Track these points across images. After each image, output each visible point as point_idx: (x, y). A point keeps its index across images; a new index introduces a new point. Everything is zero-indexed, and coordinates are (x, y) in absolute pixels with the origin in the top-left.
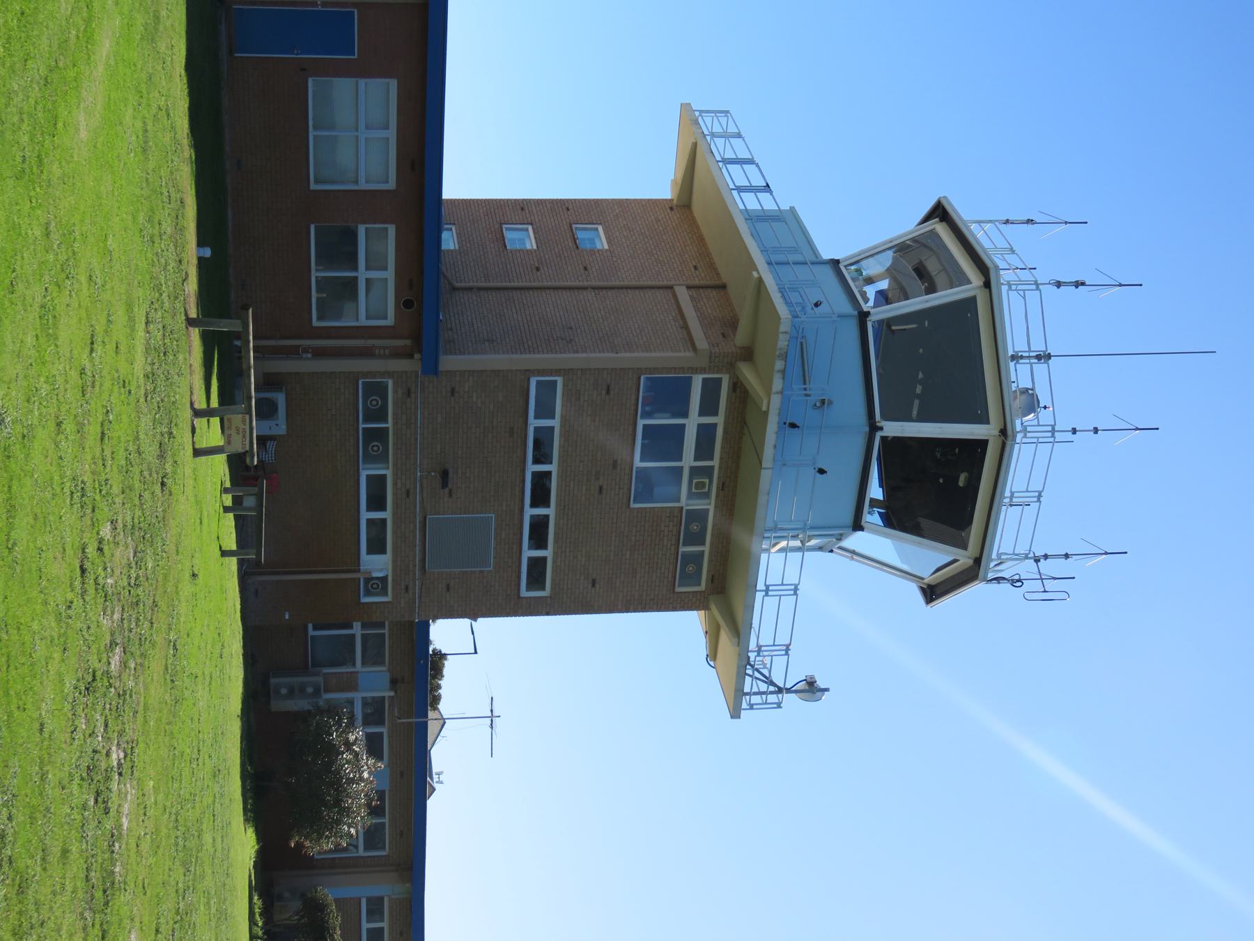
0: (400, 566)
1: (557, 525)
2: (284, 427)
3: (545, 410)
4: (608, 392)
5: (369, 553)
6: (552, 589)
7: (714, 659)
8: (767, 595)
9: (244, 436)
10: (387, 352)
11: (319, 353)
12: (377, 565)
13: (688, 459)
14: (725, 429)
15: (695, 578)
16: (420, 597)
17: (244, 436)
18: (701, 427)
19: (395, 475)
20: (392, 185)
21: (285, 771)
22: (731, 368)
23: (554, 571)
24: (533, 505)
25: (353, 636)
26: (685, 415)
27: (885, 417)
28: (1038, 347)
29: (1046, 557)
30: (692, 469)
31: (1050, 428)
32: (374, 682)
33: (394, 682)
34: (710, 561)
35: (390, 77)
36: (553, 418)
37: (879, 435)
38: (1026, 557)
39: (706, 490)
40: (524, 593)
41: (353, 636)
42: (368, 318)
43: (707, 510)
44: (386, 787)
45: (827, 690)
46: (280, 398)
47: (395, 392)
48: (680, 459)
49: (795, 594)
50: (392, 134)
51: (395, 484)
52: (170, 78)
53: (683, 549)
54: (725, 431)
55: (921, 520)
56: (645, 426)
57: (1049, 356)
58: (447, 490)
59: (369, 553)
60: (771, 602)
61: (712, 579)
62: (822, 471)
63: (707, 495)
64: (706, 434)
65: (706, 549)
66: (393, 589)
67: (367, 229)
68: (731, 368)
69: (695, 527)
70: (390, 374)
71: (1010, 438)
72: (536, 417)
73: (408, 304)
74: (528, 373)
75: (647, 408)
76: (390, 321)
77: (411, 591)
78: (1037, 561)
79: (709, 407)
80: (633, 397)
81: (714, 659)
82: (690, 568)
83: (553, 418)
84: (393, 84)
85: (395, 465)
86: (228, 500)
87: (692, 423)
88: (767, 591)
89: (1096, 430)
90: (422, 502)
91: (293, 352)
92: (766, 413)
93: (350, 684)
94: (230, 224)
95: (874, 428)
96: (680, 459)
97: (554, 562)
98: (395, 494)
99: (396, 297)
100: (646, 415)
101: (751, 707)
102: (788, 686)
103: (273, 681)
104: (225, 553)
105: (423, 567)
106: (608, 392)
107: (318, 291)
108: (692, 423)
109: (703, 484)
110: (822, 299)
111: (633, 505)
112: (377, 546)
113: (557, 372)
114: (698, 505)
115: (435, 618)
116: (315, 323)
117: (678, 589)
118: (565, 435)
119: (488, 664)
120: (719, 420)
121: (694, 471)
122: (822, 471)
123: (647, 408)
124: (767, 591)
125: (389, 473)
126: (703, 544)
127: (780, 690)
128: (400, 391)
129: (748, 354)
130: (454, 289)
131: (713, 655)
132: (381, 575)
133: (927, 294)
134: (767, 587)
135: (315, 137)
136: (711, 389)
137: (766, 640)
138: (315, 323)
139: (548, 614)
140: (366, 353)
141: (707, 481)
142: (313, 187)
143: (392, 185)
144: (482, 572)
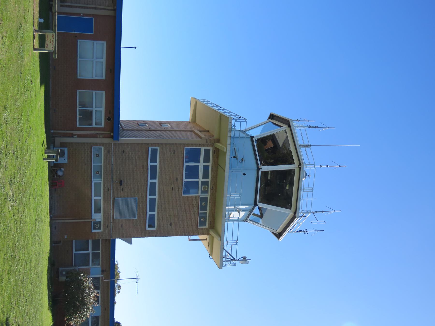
0: (106, 218)
1: (158, 202)
2: (67, 160)
3: (154, 160)
5: (95, 213)
6: (157, 226)
7: (212, 255)
8: (227, 244)
9: (53, 44)
11: (79, 136)
12: (98, 217)
13: (200, 179)
15: (204, 223)
17: (53, 44)
19: (104, 183)
20: (104, 78)
21: (64, 296)
26: (199, 162)
27: (260, 202)
28: (306, 143)
29: (316, 212)
30: (202, 182)
32: (96, 270)
33: (103, 271)
34: (209, 216)
35: (104, 40)
36: (156, 162)
37: (260, 171)
40: (148, 229)
41: (89, 254)
42: (96, 76)
44: (99, 314)
46: (66, 150)
47: (104, 151)
48: (198, 178)
49: (236, 244)
50: (104, 60)
51: (104, 186)
52: (38, 220)
53: (200, 212)
54: (212, 168)
55: (281, 145)
56: (187, 166)
57: (310, 145)
59: (95, 213)
60: (230, 224)
61: (210, 223)
62: (244, 174)
63: (207, 192)
64: (206, 168)
65: (208, 212)
68: (213, 145)
72: (150, 195)
73: (109, 119)
74: (148, 145)
75: (187, 160)
76: (103, 126)
78: (313, 213)
79: (206, 160)
81: (212, 255)
83: (155, 211)
84: (105, 43)
85: (104, 178)
86: (46, 156)
87: (201, 165)
89: (322, 212)
90: (113, 193)
91: (70, 135)
92: (226, 152)
94: (51, 88)
95: (259, 169)
96: (198, 178)
97: (158, 216)
98: (104, 190)
99: (105, 117)
100: (186, 162)
101: (226, 265)
102: (238, 258)
105: (113, 218)
106: (174, 153)
107: (79, 115)
108: (201, 165)
109: (206, 187)
111: (183, 195)
112: (98, 211)
113: (157, 145)
114: (204, 195)
115: (117, 238)
116: (78, 126)
117: (199, 227)
118: (161, 168)
119: (132, 255)
120: (210, 164)
122: (244, 174)
124: (227, 243)
126: (206, 210)
127: (234, 260)
129: (218, 141)
130: (123, 130)
131: (211, 254)
132: (99, 220)
136: (207, 152)
137: (229, 239)
138: (78, 126)
139: (156, 236)
140: (95, 136)
142: (78, 78)
143: (104, 78)
144: (133, 220)
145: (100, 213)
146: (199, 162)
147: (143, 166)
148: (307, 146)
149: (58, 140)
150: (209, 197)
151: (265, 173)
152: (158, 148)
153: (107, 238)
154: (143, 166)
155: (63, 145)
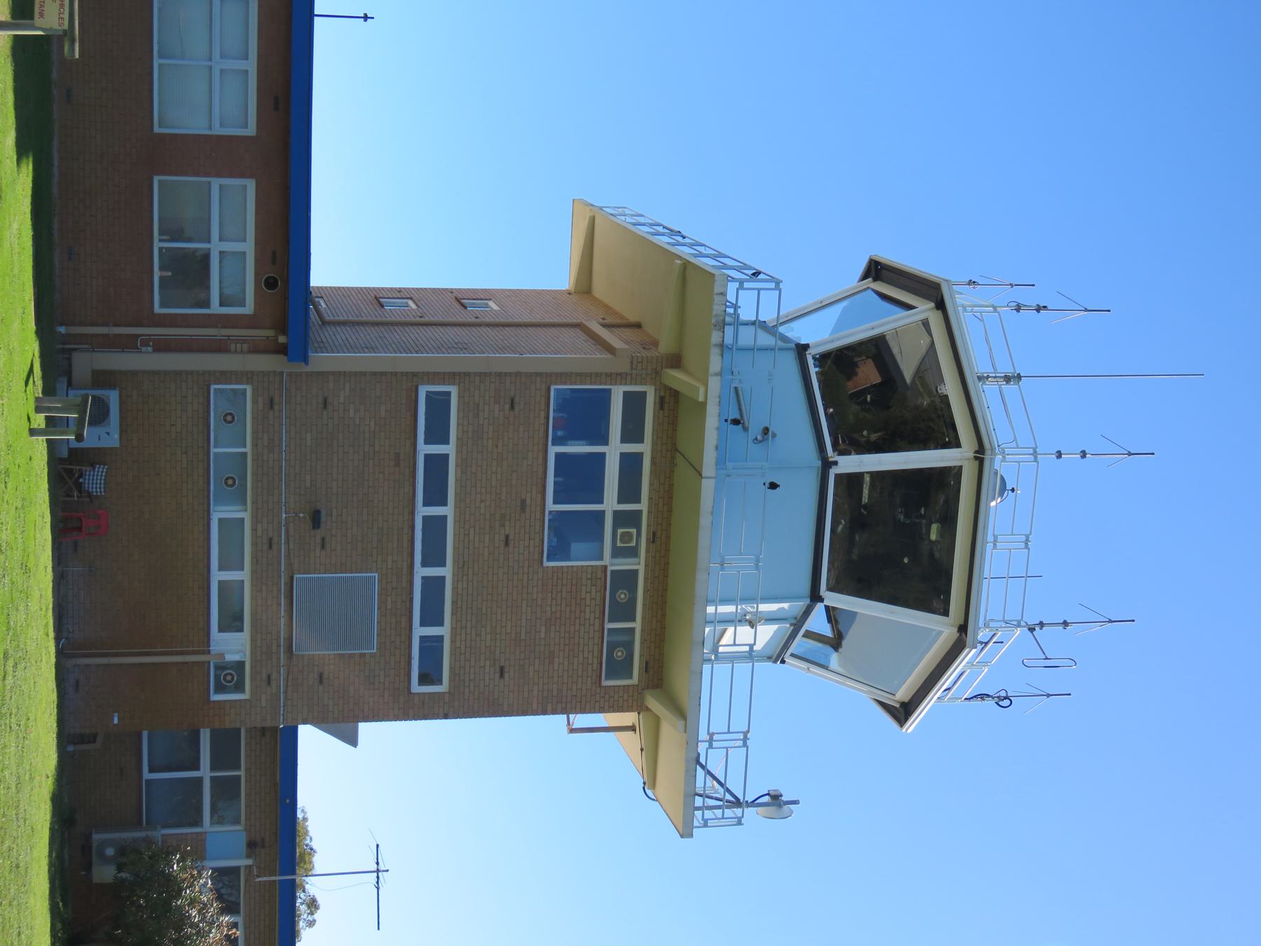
0: (262, 649)
1: (454, 589)
2: (117, 436)
3: (438, 433)
4: (512, 407)
5: (221, 630)
8: (711, 746)
10: (245, 346)
11: (162, 346)
12: (232, 646)
13: (610, 502)
14: (653, 458)
15: (623, 669)
16: (286, 692)
17: (62, 6)
18: (624, 456)
20: (251, 130)
22: (657, 374)
23: (452, 654)
24: (425, 564)
25: (199, 781)
26: (605, 441)
28: (1005, 368)
29: (1042, 625)
31: (1031, 451)
32: (226, 842)
33: (251, 845)
34: (643, 642)
37: (833, 472)
38: (1019, 625)
39: (633, 544)
40: (416, 688)
41: (199, 781)
42: (221, 305)
43: (636, 571)
45: (795, 802)
46: (113, 397)
47: (255, 402)
48: (600, 501)
49: (745, 745)
50: (251, 65)
51: (254, 530)
53: (608, 626)
55: (908, 375)
56: (559, 456)
57: (1019, 377)
58: (319, 533)
59: (221, 630)
60: (722, 669)
61: (646, 667)
62: (773, 486)
63: (633, 552)
64: (630, 464)
65: (637, 625)
66: (252, 679)
67: (221, 187)
69: (622, 596)
70: (246, 376)
71: (988, 452)
72: (424, 564)
73: (271, 283)
74: (415, 378)
75: (560, 433)
76: (248, 308)
77: (274, 684)
78: (1032, 630)
79: (632, 432)
80: (543, 414)
81: (653, 786)
82: (619, 654)
85: (254, 502)
86: (39, 421)
87: (614, 450)
88: (711, 741)
89: (1065, 624)
90: (288, 556)
91: (129, 344)
93: (198, 853)
94: (55, 171)
95: (827, 465)
96: (601, 502)
97: (453, 641)
98: (254, 544)
99: (256, 274)
103: (97, 837)
104: (33, 432)
106: (512, 407)
107: (161, 269)
108: (614, 450)
109: (630, 534)
110: (751, 444)
112: (232, 622)
114: (624, 564)
115: (305, 723)
116: (157, 309)
117: (605, 683)
118: (463, 465)
120: (645, 448)
121: (623, 519)
122: (773, 486)
123: (560, 433)
124: (711, 741)
125: (246, 516)
127: (737, 803)
128: (260, 399)
129: (676, 361)
130: (324, 323)
131: (650, 781)
132: (236, 658)
133: (855, 614)
134: (711, 735)
135: (160, 66)
136: (634, 404)
137: (718, 725)
138: (157, 309)
139: (446, 717)
140: (219, 347)
141: (634, 531)
142: (157, 129)
143: (251, 130)
145: (241, 630)
146: (605, 441)
147: (397, 455)
148: (1008, 379)
149: (84, 363)
150: (641, 569)
151: (851, 482)
152: (454, 390)
153: (268, 724)
154: (397, 455)
155: (103, 379)
